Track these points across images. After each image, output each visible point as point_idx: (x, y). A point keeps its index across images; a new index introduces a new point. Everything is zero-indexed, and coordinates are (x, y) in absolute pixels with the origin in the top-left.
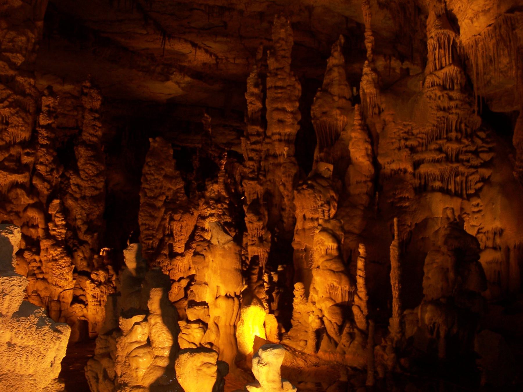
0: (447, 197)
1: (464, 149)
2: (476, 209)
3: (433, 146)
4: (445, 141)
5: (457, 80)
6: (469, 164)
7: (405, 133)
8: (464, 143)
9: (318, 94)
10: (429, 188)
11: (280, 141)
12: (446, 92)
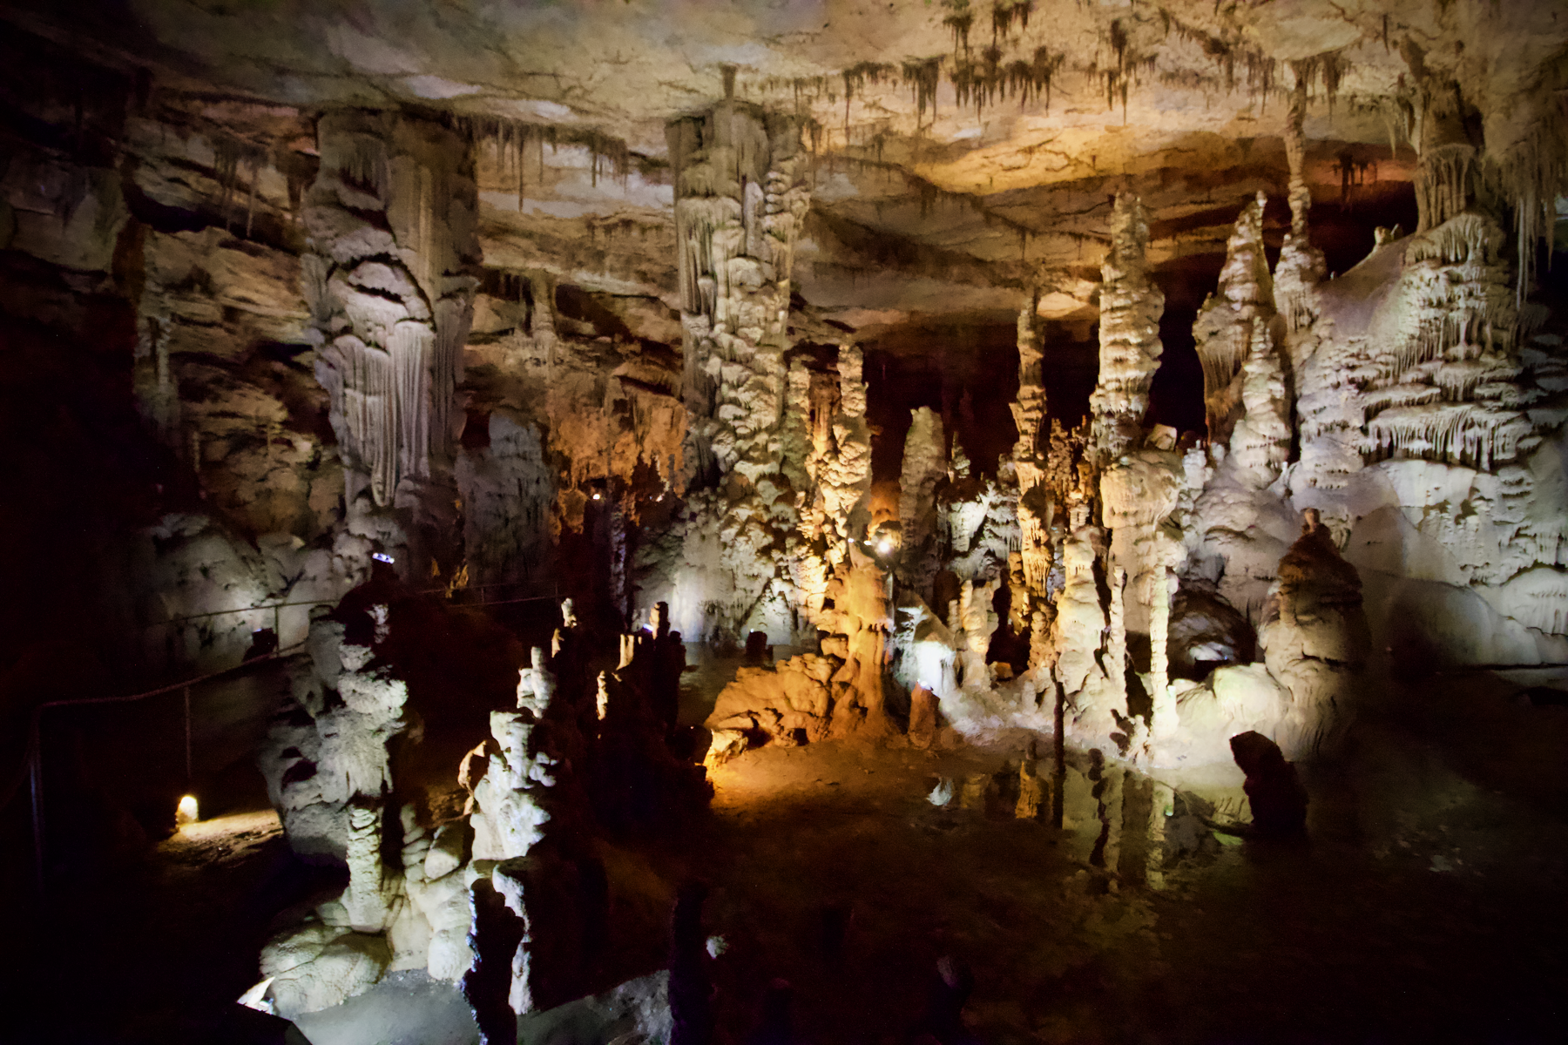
0: (1440, 469)
1: (1486, 376)
2: (1514, 491)
3: (1410, 376)
4: (1439, 364)
5: (1476, 239)
6: (1501, 404)
7: (1352, 355)
8: (1485, 365)
9: (1206, 302)
10: (1398, 453)
11: (1119, 390)
12: (1445, 269)
